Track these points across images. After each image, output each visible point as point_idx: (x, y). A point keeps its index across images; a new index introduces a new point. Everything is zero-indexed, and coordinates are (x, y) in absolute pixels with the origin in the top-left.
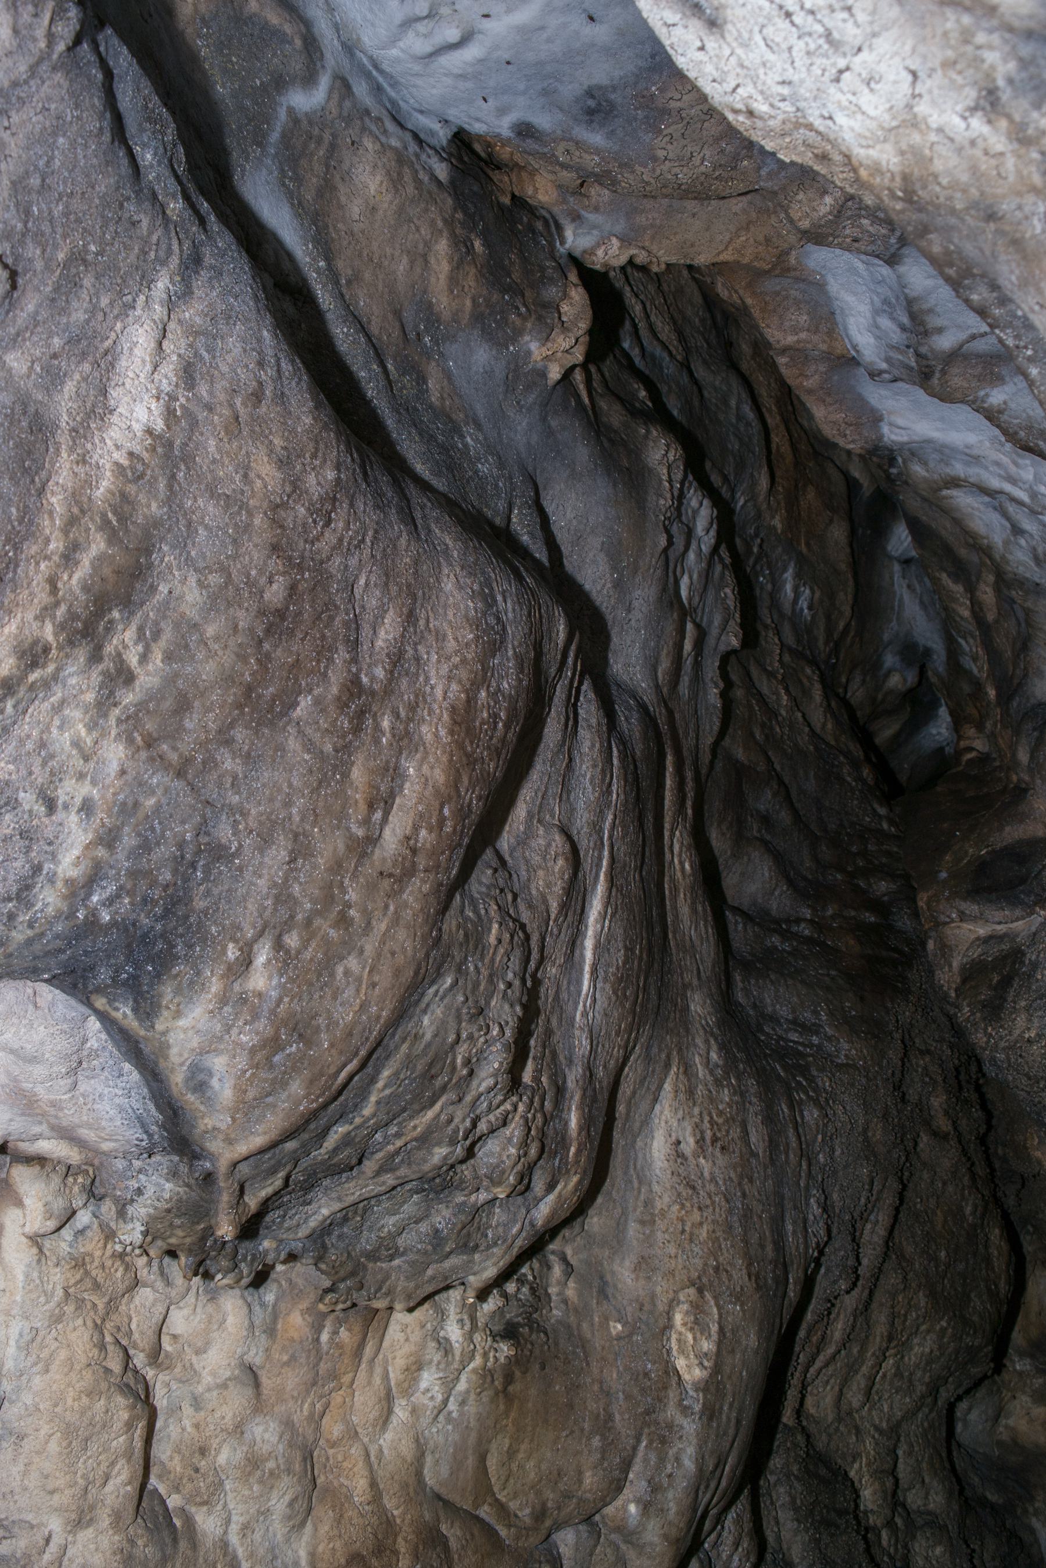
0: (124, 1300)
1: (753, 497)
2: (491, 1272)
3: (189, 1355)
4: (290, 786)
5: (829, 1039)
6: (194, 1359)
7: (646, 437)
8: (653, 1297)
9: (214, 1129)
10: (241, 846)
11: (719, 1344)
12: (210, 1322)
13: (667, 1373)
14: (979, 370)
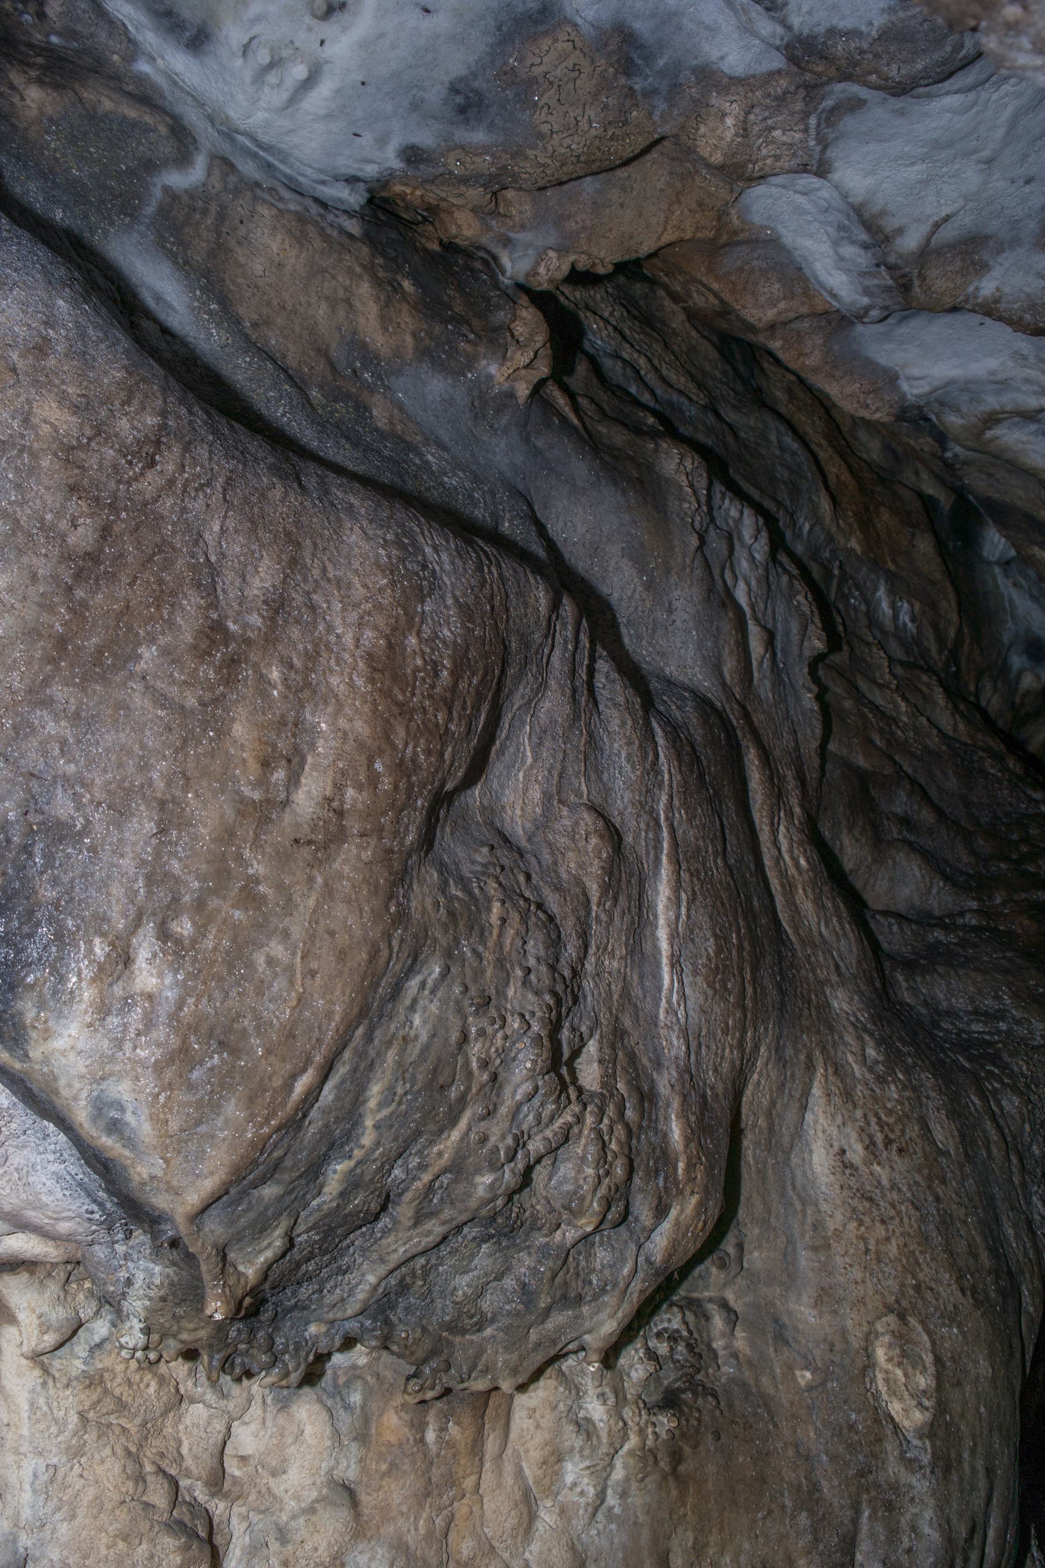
0: (168, 1423)
1: (818, 521)
2: (608, 1326)
3: (265, 1478)
4: (143, 747)
5: (1019, 1022)
6: (272, 1482)
7: (656, 451)
8: (844, 1333)
9: (152, 1178)
10: (88, 822)
11: (938, 1377)
12: (282, 1436)
13: (877, 1421)
14: (958, 264)
